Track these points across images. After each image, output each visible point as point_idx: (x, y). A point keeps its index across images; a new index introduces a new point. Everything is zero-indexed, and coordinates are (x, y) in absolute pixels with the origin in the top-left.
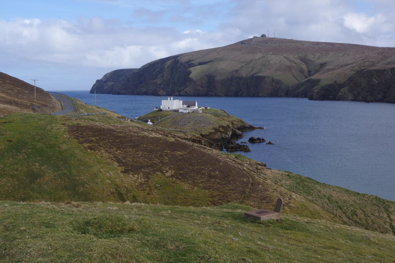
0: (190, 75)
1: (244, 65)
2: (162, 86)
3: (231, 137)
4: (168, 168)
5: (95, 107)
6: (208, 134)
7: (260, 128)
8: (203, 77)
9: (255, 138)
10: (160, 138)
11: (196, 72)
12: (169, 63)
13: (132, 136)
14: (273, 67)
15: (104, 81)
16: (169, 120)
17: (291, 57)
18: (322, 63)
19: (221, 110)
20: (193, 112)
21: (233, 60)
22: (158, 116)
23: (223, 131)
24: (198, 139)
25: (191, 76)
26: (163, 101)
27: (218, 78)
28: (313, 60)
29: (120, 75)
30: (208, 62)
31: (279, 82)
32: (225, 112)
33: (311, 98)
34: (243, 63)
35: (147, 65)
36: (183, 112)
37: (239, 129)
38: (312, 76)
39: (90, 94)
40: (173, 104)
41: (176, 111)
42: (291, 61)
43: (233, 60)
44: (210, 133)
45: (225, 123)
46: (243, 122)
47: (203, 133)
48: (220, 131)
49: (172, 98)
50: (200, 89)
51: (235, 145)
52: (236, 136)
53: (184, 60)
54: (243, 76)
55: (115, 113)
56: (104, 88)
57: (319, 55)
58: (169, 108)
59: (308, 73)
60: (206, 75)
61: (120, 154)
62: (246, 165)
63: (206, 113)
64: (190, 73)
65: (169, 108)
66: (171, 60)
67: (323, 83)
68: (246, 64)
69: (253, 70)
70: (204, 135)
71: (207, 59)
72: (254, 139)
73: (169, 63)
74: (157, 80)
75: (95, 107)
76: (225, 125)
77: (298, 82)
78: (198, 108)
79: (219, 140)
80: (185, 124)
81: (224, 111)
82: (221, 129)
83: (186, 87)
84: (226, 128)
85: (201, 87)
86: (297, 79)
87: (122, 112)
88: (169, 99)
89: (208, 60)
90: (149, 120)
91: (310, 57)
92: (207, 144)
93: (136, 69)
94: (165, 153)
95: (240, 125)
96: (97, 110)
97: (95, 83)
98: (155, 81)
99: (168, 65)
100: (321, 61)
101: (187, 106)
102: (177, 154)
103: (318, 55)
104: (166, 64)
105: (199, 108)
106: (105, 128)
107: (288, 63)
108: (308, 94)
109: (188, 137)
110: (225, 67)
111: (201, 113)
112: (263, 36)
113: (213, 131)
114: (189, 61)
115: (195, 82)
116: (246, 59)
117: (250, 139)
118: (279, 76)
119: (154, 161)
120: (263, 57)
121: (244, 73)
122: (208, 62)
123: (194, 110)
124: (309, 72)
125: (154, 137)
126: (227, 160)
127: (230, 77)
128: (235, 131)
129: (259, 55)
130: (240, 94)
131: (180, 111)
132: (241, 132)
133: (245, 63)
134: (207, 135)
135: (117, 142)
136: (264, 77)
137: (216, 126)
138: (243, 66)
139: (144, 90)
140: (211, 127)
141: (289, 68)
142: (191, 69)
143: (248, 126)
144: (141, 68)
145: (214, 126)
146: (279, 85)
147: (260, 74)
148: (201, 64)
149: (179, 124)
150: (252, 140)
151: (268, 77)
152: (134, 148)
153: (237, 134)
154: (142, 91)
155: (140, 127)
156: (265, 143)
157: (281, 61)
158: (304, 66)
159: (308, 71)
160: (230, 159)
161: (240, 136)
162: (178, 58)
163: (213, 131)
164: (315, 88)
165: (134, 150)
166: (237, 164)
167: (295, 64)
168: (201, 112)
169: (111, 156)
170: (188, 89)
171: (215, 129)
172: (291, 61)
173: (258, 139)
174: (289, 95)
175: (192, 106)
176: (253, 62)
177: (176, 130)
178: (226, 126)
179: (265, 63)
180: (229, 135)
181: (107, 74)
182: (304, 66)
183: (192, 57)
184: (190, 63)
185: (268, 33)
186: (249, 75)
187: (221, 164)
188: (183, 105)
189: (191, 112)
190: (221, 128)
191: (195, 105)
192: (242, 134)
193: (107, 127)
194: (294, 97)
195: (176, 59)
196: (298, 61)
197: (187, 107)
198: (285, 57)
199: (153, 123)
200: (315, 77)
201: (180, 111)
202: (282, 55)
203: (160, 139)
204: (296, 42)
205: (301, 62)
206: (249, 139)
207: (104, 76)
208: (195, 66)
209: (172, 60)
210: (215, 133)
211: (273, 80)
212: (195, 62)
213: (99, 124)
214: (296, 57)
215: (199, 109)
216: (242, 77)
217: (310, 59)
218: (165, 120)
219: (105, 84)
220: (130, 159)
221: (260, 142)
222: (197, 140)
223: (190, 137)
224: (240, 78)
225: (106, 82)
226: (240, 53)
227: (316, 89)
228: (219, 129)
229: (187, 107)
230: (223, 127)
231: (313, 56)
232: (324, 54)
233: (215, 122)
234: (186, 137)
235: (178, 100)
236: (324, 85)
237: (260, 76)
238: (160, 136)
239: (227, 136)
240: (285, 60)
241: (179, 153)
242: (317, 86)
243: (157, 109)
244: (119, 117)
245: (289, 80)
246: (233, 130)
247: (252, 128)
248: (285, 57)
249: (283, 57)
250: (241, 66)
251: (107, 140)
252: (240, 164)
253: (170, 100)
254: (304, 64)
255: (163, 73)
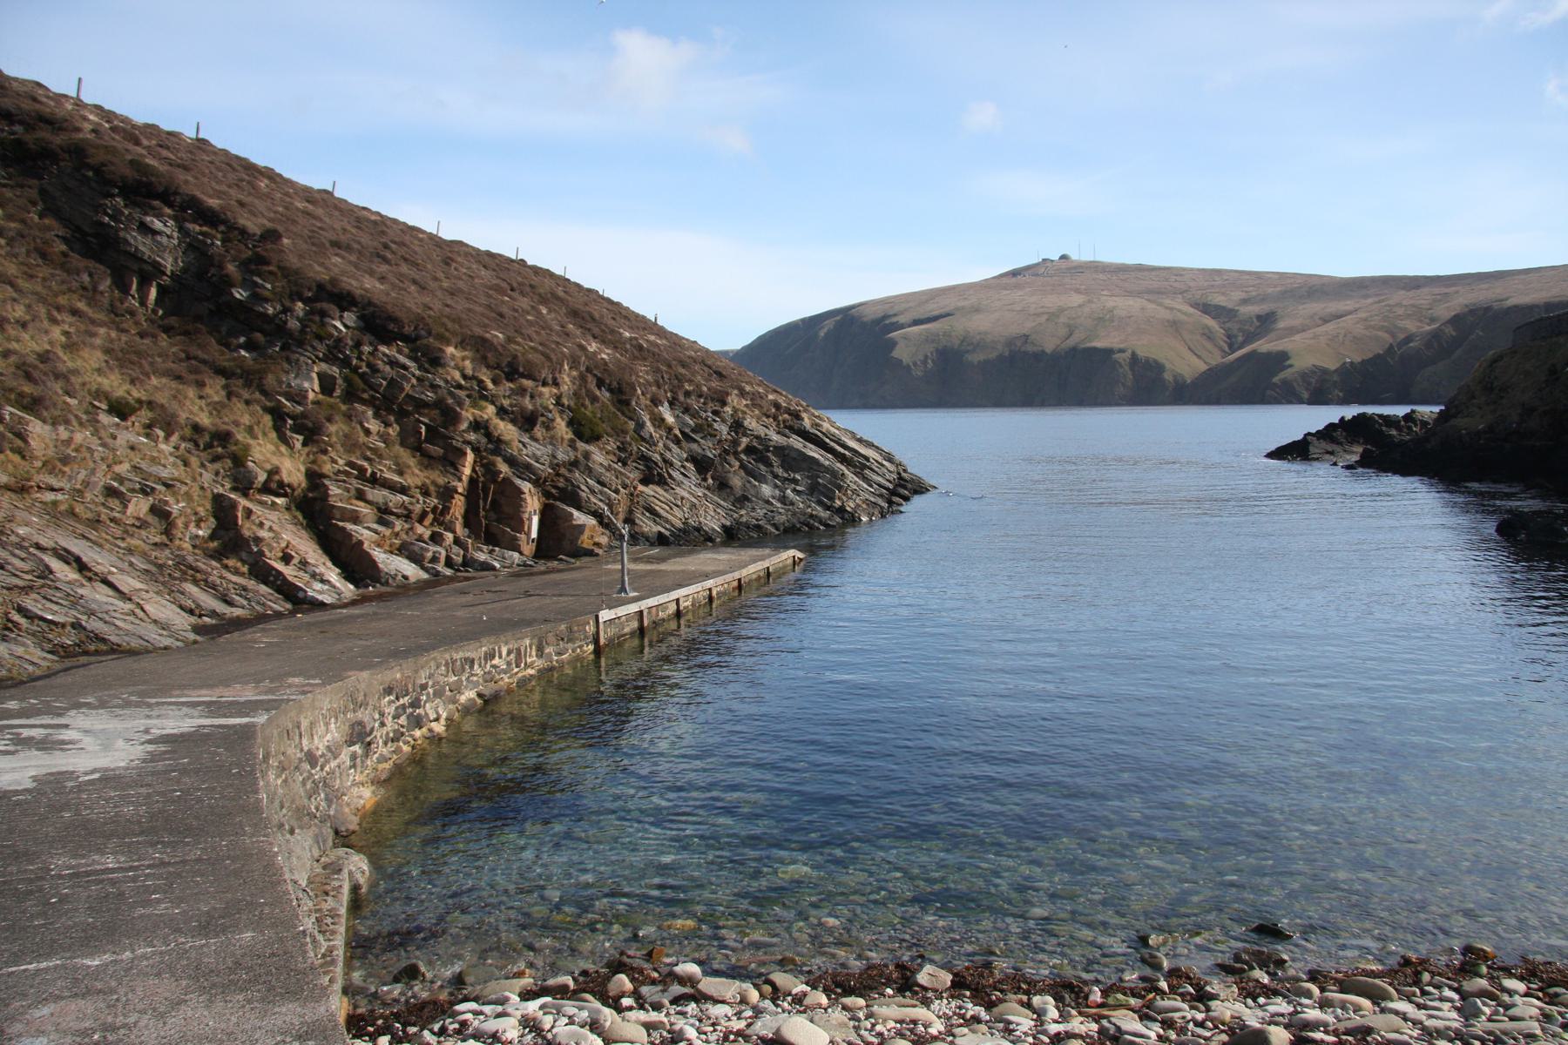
11: (908, 347)
14: (1132, 331)
35: (1462, 300)
53: (870, 314)
54: (1048, 351)
64: (893, 344)
71: (933, 308)
73: (829, 324)
77: (1203, 367)
89: (936, 313)
112: (1064, 257)
118: (1148, 346)
120: (1090, 301)
131: (976, 583)
136: (1109, 352)
147: (1098, 344)
148: (916, 322)
151: (1121, 351)
208: (902, 327)
245: (1186, 363)
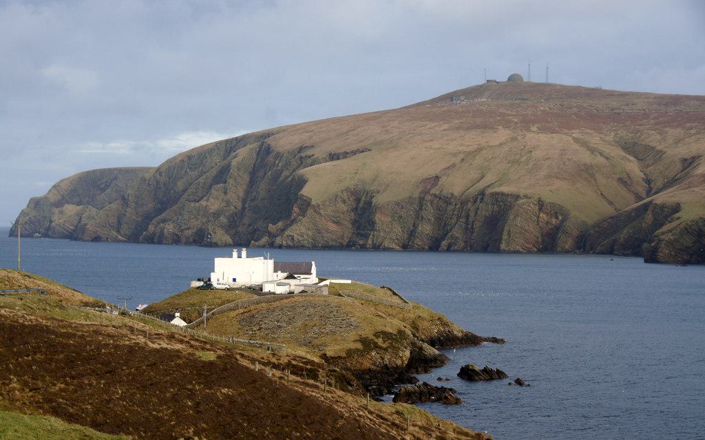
0: (302, 188)
1: (457, 160)
2: (223, 220)
3: (407, 365)
4: (191, 431)
5: (16, 275)
6: (344, 355)
7: (495, 340)
8: (339, 194)
9: (477, 368)
10: (178, 351)
11: (321, 183)
12: (243, 153)
13: (99, 346)
15: (52, 201)
16: (233, 314)
17: (595, 140)
18: (685, 157)
19: (384, 287)
20: (303, 292)
21: (426, 148)
22: (205, 302)
23: (384, 346)
24: (309, 367)
25: (306, 191)
26: (216, 259)
27: (379, 200)
28: (659, 148)
29: (103, 186)
30: (354, 153)
31: (558, 211)
32: (395, 294)
33: (652, 258)
34: (455, 155)
36: (274, 293)
37: (432, 343)
38: (656, 193)
39: (10, 238)
40: (240, 270)
41: (257, 290)
42: (592, 151)
43: (426, 148)
44: (350, 353)
45: (392, 325)
46: (445, 324)
47: (329, 354)
48: (376, 346)
49: (244, 253)
50: (332, 227)
51: (419, 387)
52: (421, 362)
54: (456, 194)
55: (76, 293)
56: (51, 222)
57: (677, 132)
58: (234, 280)
59: (644, 184)
60: (347, 189)
61: (65, 392)
62: (411, 428)
63: (340, 295)
64: (302, 182)
65: (234, 280)
66: (251, 144)
67: (687, 215)
68: (463, 160)
69: (483, 177)
70: (332, 358)
72: (474, 371)
74: (208, 200)
75: (16, 275)
76: (391, 331)
77: (610, 211)
78: (319, 283)
79: (374, 371)
80: (280, 327)
81: (391, 290)
82: (380, 341)
83: (293, 222)
84: (395, 339)
85: (334, 222)
86: (611, 203)
87: (112, 297)
88: (235, 254)
89: (354, 147)
90: (177, 314)
91: (652, 139)
92: (333, 382)
93: (147, 169)
94: (189, 390)
95: (435, 331)
96: (23, 281)
97: (24, 206)
98: (203, 203)
99: (239, 159)
100: (684, 151)
101: (285, 274)
102: (218, 394)
103: (673, 133)
104: (236, 156)
105: (321, 280)
106: (26, 323)
107: (586, 157)
108: (645, 245)
109: (281, 362)
110: (399, 170)
111: (325, 296)
112: (513, 79)
113: (359, 346)
114: (301, 149)
115: (316, 209)
116: (462, 145)
117: (462, 369)
118: (559, 192)
119: (154, 413)
120: (513, 139)
121: (456, 185)
122: (354, 153)
123: (305, 285)
124: (648, 181)
125: (162, 348)
126: (361, 413)
127: (416, 195)
128: (421, 349)
129: (503, 134)
130: (444, 243)
131: (266, 289)
132: (437, 352)
133: (461, 156)
134: (340, 357)
135: (57, 361)
137: (368, 333)
138: (454, 165)
139: (169, 228)
140: (353, 335)
141: (586, 173)
142: (305, 171)
143: (460, 335)
144: (162, 165)
145: (360, 332)
146: (557, 218)
147: (505, 189)
148: (333, 157)
149: (263, 326)
150: (467, 374)
152: (101, 378)
153: (424, 355)
154: (165, 230)
155: (136, 326)
156: (506, 381)
157: (564, 150)
158: (633, 167)
159: (643, 179)
160: (371, 413)
161: (436, 362)
162: (269, 141)
163: (359, 346)
164: (665, 228)
165: (103, 381)
166: (388, 425)
167: (607, 158)
168: (326, 292)
169: (40, 398)
170: (300, 230)
171: (364, 341)
172: (592, 151)
173: (486, 370)
174: (587, 248)
175: (302, 276)
176: (484, 152)
177: (252, 342)
178: (395, 332)
179: (518, 157)
180: (404, 359)
181: (62, 181)
182: (633, 167)
183: (311, 137)
184: (303, 155)
185: (529, 69)
186: (470, 190)
187: (341, 423)
188: (275, 271)
189: (297, 290)
190: (381, 340)
191: (310, 274)
192: (440, 355)
193: (31, 320)
194: (603, 253)
195: (263, 143)
196: (617, 152)
197: (287, 278)
198: (576, 140)
199: (190, 322)
200: (660, 198)
201: (266, 289)
202: (566, 134)
203: (177, 354)
204: (611, 94)
205: (623, 154)
206: (458, 371)
207: (54, 187)
209: (251, 146)
210: (361, 353)
211: (541, 205)
212: (317, 153)
213: (11, 312)
214: (608, 138)
215: (322, 284)
216: (452, 194)
217: (650, 144)
218: (222, 312)
219: (56, 210)
220: (89, 407)
221: (491, 379)
222: (306, 369)
223: (286, 361)
224: (447, 200)
225: (59, 204)
226: (446, 126)
227: (667, 232)
228: (376, 340)
229: (287, 278)
230: (386, 335)
231: (659, 137)
232: (693, 132)
233: (366, 322)
234: (274, 360)
235: (262, 258)
236: (693, 221)
237: (503, 194)
238: (177, 348)
239: (399, 362)
240: (576, 147)
241: (225, 391)
242: (670, 222)
243: (201, 284)
244: (86, 304)
245: (586, 205)
246: (413, 344)
247: (471, 340)
248: (576, 140)
249: (572, 141)
250: (447, 165)
251: (28, 356)
252: (397, 426)
253: (240, 256)
254: (632, 158)
255: (225, 182)
